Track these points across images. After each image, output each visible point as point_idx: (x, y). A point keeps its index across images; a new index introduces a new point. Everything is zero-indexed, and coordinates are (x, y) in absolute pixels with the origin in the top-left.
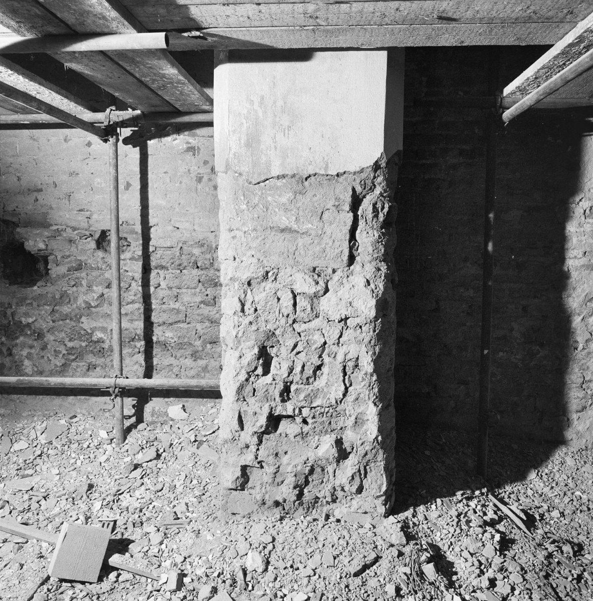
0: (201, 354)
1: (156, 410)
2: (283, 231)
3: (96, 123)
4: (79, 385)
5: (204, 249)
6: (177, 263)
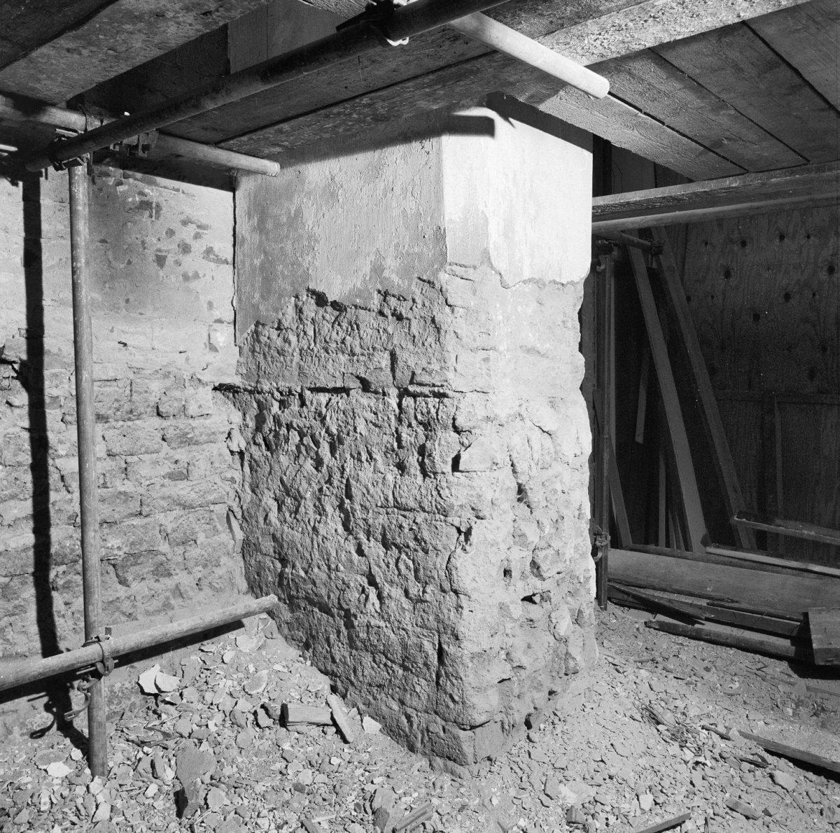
0: (167, 567)
1: (116, 690)
2: (528, 351)
3: (61, 128)
4: (68, 666)
5: (168, 382)
6: (127, 407)
